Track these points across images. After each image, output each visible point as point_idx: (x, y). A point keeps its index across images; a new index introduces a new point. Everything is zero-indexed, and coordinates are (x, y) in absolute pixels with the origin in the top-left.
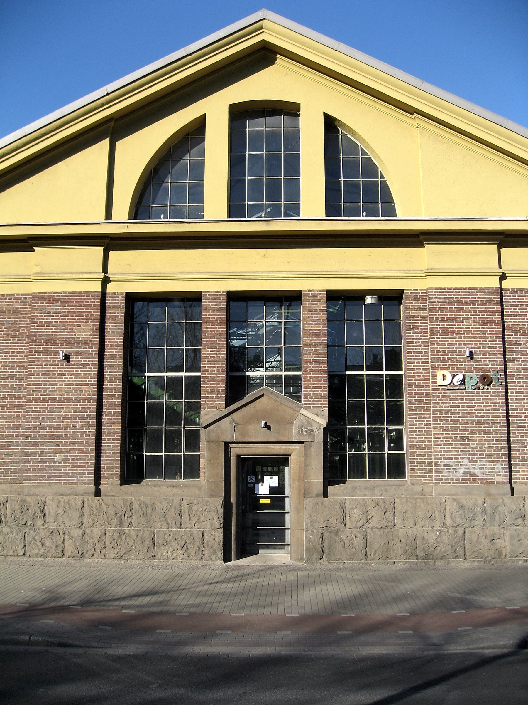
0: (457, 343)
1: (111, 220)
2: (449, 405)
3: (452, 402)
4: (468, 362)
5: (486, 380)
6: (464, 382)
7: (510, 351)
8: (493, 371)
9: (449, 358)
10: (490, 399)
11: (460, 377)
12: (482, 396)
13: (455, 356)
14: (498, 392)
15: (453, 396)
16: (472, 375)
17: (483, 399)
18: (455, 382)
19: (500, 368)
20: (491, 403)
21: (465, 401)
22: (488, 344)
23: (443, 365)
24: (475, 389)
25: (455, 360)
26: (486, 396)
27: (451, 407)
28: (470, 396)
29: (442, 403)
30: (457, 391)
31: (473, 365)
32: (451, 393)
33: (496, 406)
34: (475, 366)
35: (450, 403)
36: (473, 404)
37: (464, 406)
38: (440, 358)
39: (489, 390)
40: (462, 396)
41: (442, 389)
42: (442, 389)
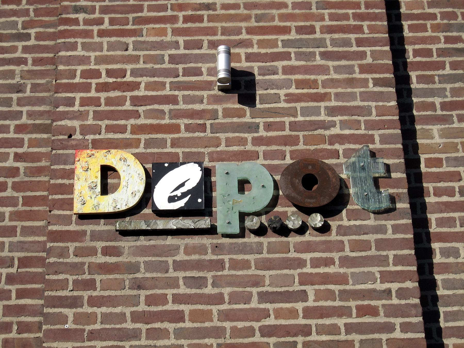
0: (181, 40)
1: (4, 306)
2: (128, 311)
3: (143, 293)
4: (228, 113)
5: (315, 190)
6: (209, 202)
7: (429, 80)
8: (348, 154)
9: (136, 101)
10: (341, 279)
11: (190, 174)
12: (301, 263)
13: (167, 92)
14: (380, 244)
15: (150, 267)
16: (245, 169)
17: (306, 279)
18: (161, 199)
19: (386, 139)
20: (345, 295)
21: (209, 290)
22: (320, 43)
23: (109, 129)
24: (261, 231)
25: (166, 108)
26: (316, 263)
27: (136, 317)
28: (235, 265)
29: (93, 302)
30: (170, 240)
31: (254, 128)
32: (143, 251)
33: (373, 311)
34: (262, 133)
35: (134, 301)
36: (254, 304)
37: (207, 316)
38: (96, 102)
39: (333, 236)
40: (198, 265)
41: (95, 236)
42: (95, 236)
